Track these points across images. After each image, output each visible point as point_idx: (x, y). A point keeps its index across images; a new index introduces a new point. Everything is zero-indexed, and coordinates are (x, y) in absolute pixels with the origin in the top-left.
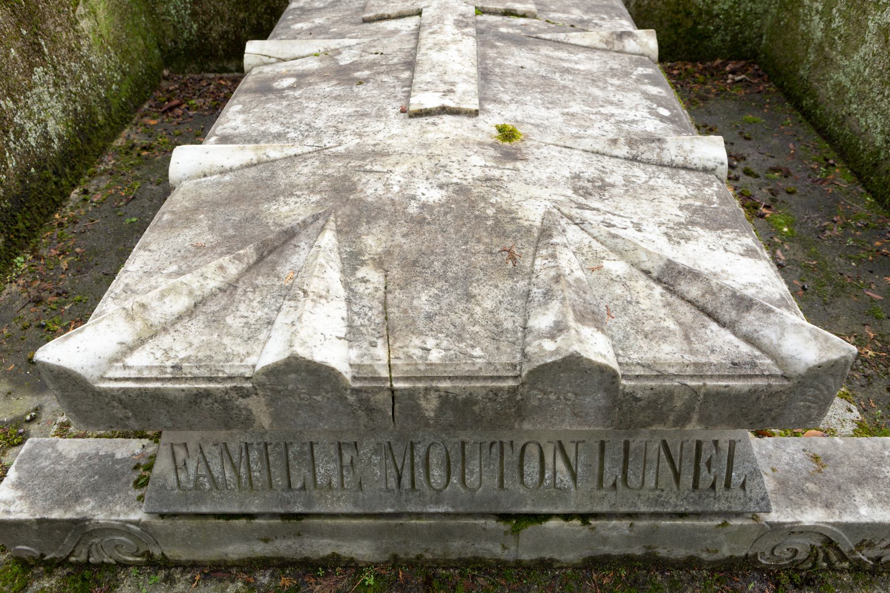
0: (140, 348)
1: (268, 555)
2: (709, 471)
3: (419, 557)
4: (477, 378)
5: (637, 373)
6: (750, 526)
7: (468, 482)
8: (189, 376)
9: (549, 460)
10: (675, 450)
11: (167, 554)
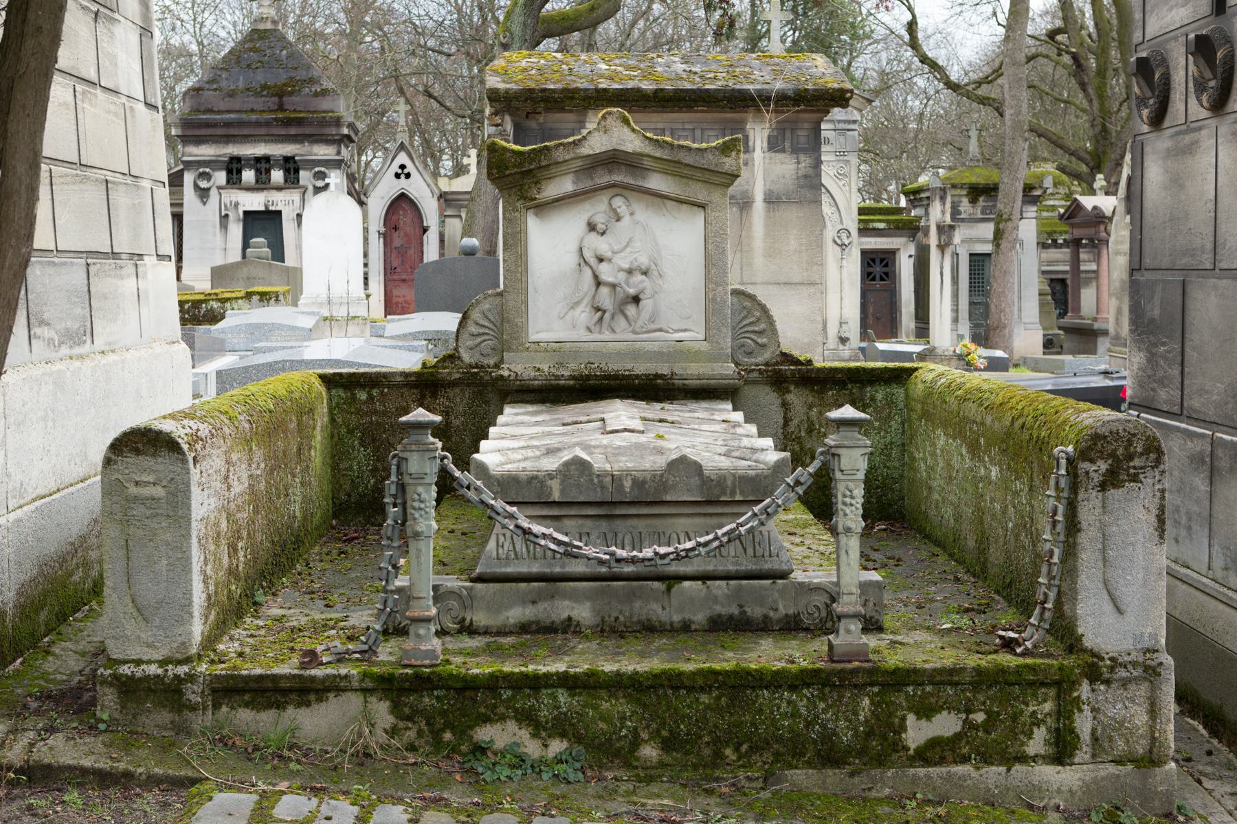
11: (475, 619)
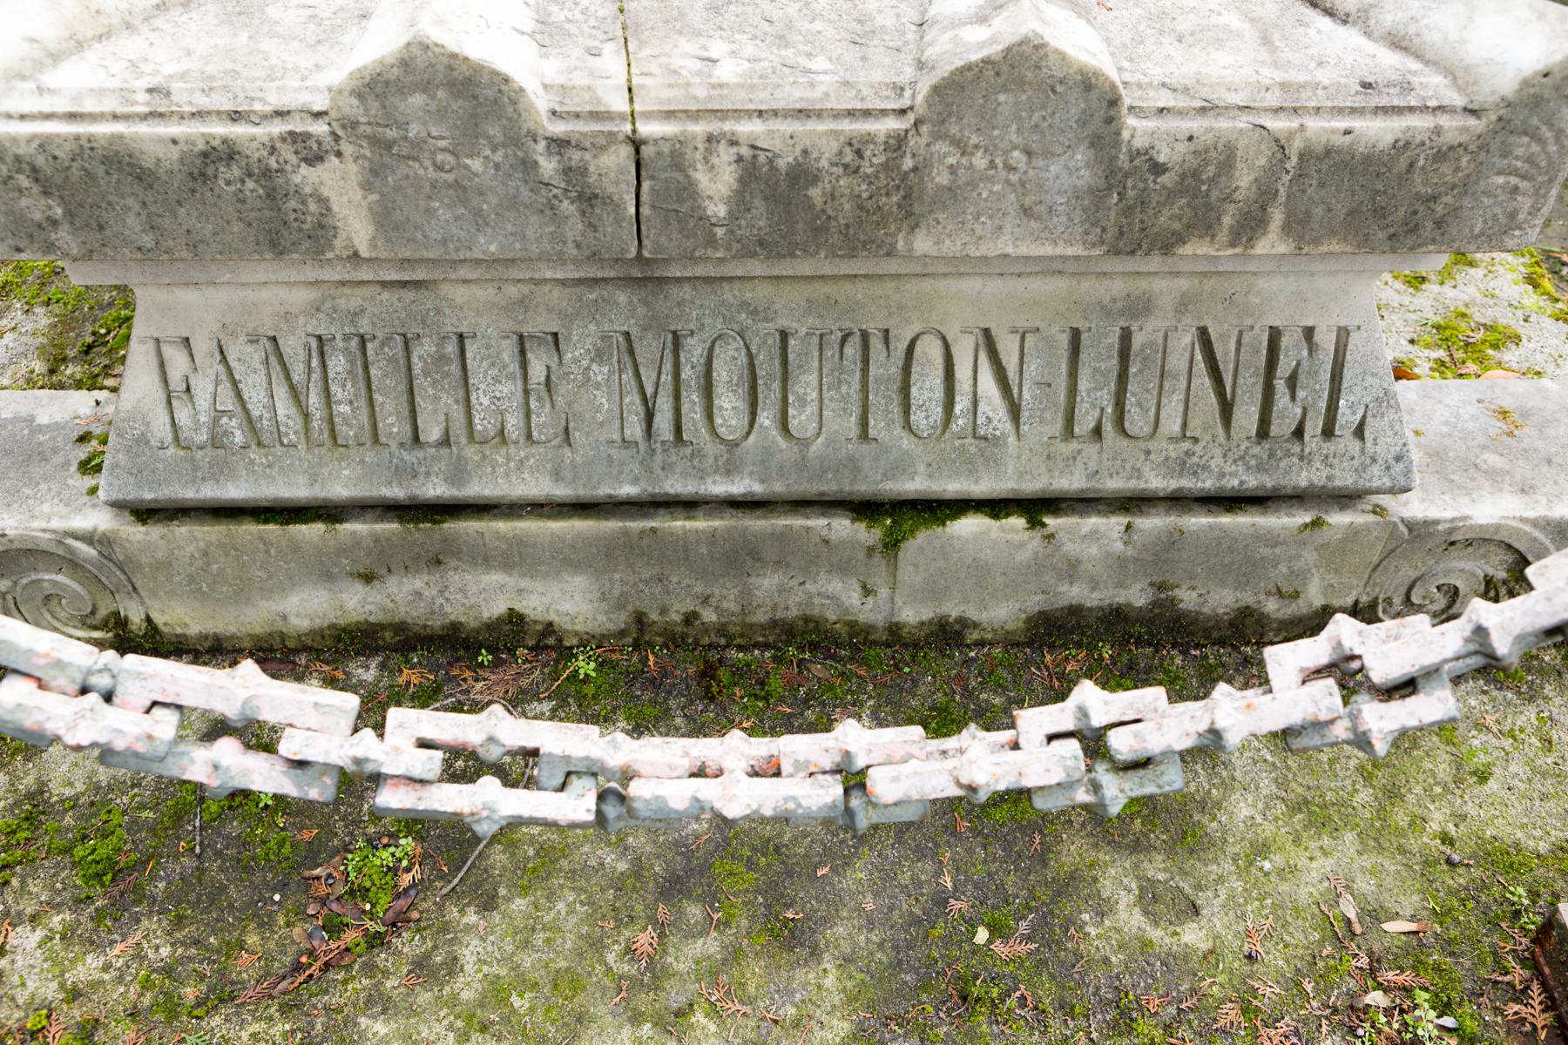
0: (74, 58)
1: (372, 619)
2: (1293, 398)
3: (690, 618)
4: (819, 114)
5: (1161, 105)
6: (1367, 528)
7: (793, 424)
8: (187, 109)
9: (963, 372)
10: (1225, 351)
11: (158, 619)
